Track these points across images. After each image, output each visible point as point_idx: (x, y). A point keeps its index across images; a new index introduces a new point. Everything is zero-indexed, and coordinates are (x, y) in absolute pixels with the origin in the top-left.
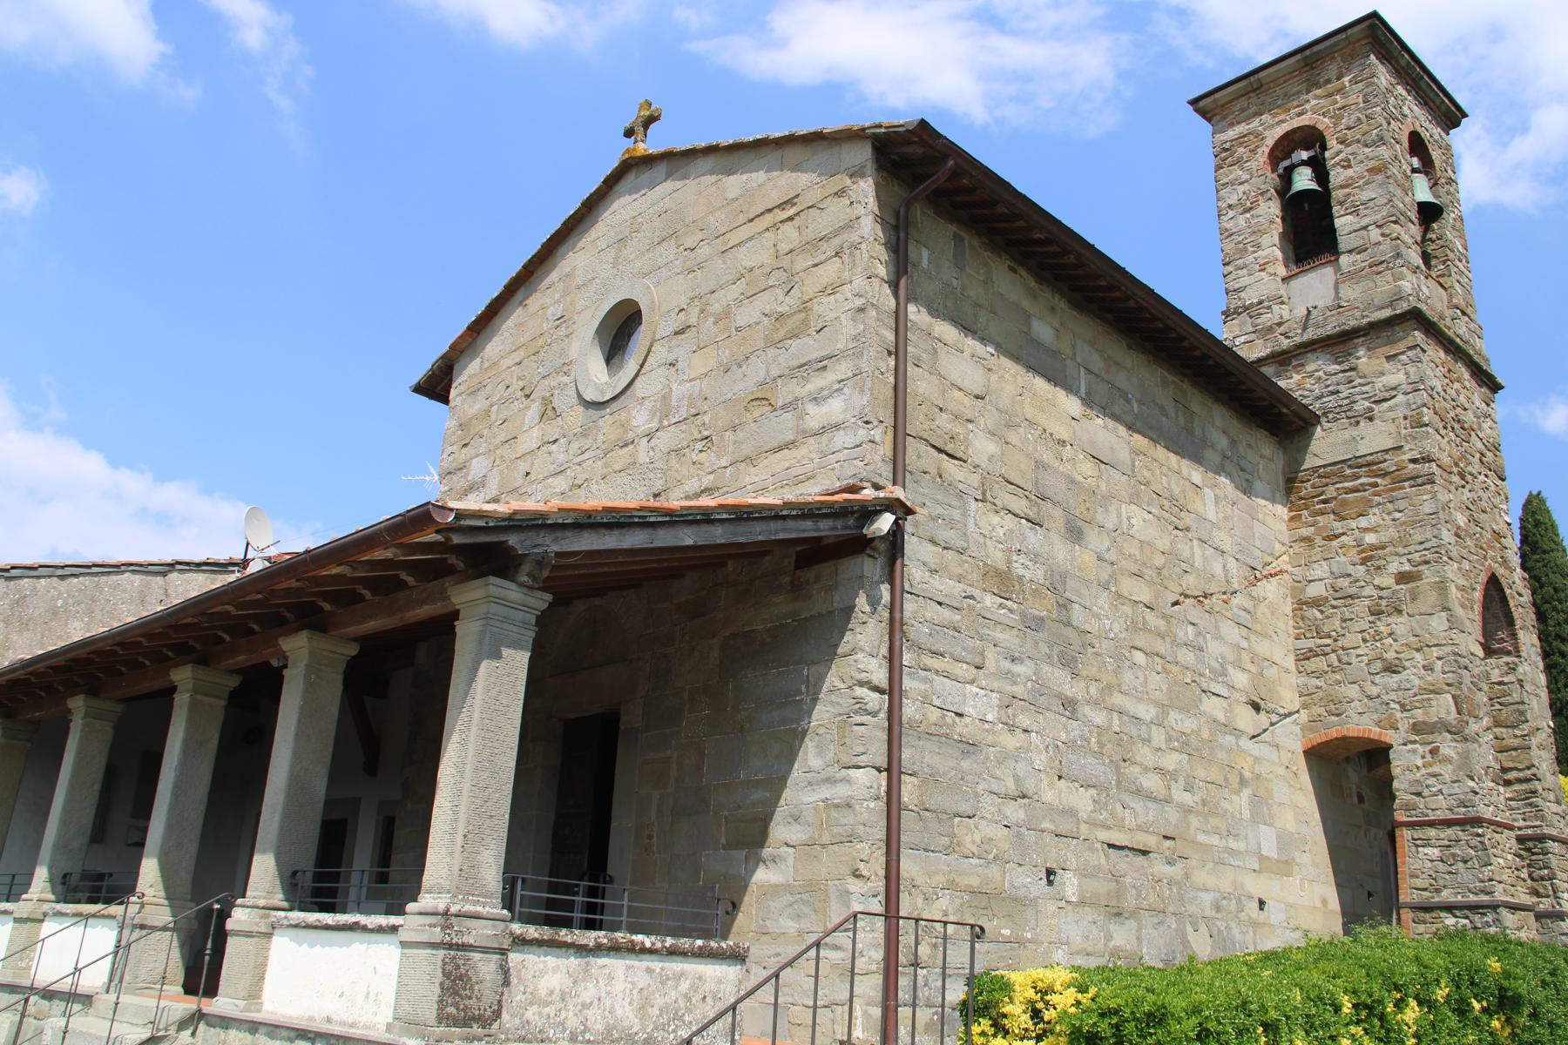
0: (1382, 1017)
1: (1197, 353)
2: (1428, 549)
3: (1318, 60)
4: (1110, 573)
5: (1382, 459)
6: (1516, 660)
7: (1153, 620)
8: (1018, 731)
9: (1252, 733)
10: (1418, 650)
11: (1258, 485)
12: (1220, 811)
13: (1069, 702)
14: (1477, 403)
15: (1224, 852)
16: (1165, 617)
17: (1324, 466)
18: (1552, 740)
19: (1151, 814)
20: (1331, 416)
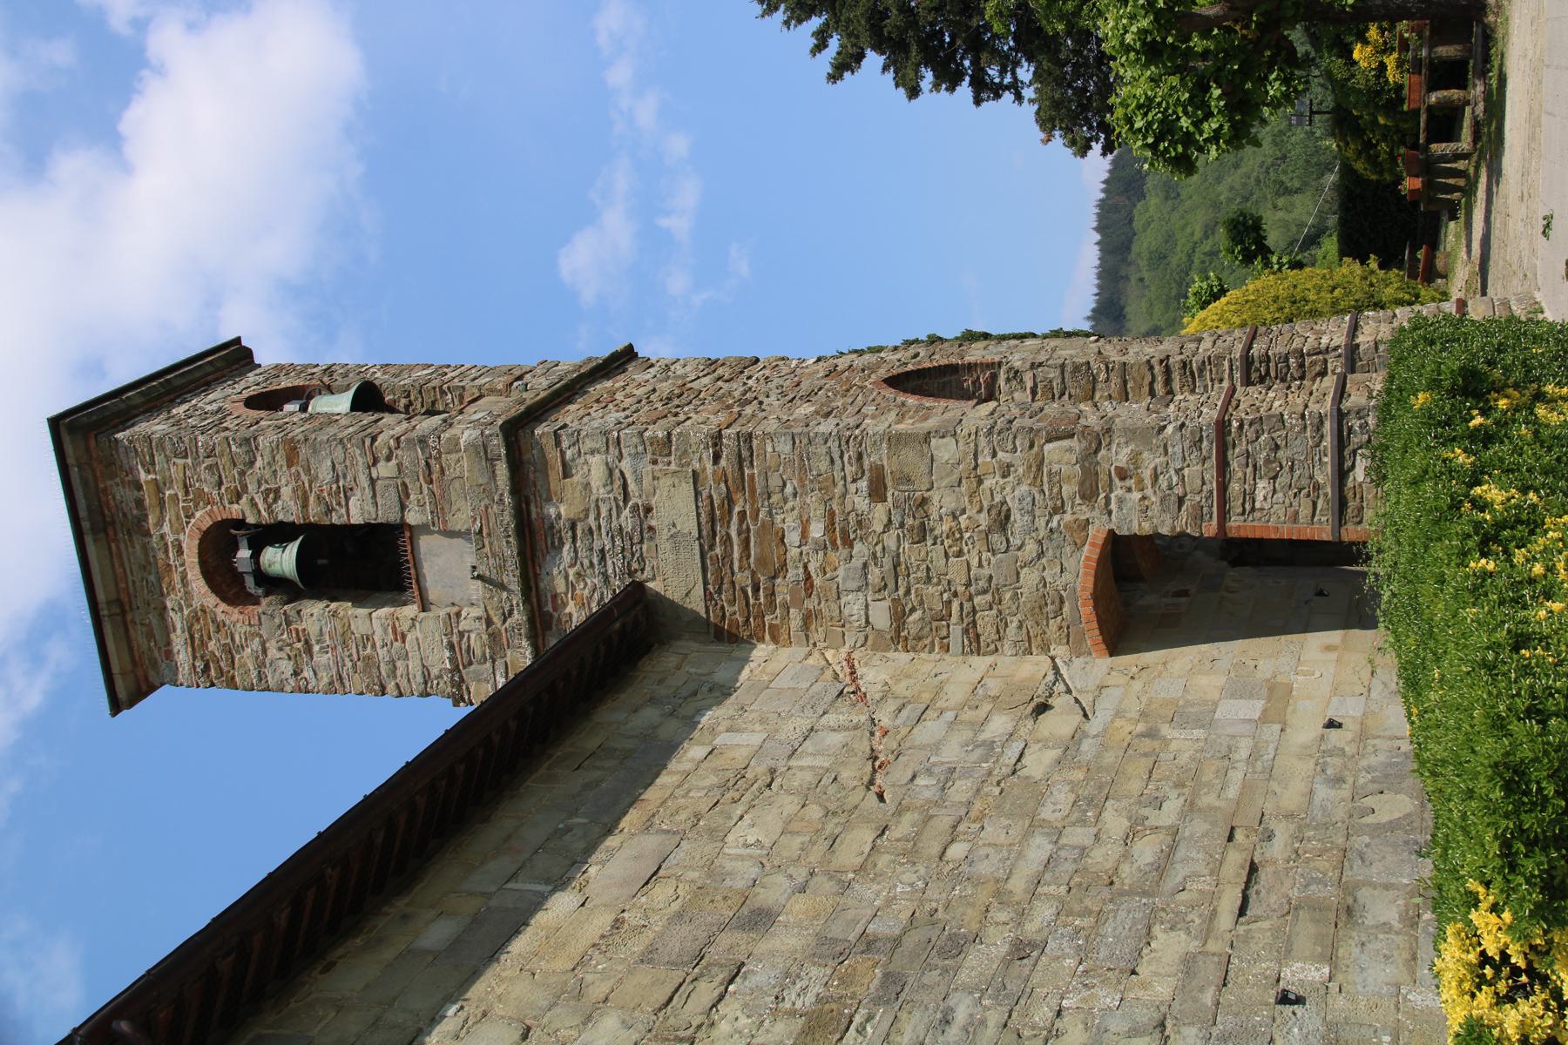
0: (1500, 525)
1: (513, 725)
2: (842, 453)
3: (102, 513)
4: (825, 879)
5: (708, 501)
6: (1004, 368)
7: (904, 827)
8: (1059, 1024)
9: (1079, 717)
10: (980, 482)
11: (721, 676)
12: (1193, 766)
13: (1018, 950)
14: (648, 376)
15: (1254, 767)
16: (900, 811)
17: (706, 583)
18: (1115, 340)
19: (1193, 855)
20: (635, 566)
